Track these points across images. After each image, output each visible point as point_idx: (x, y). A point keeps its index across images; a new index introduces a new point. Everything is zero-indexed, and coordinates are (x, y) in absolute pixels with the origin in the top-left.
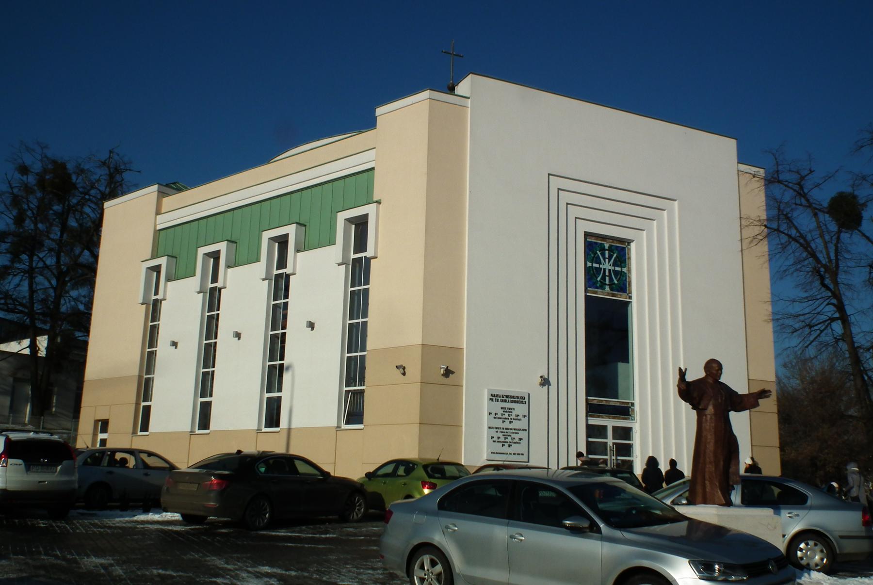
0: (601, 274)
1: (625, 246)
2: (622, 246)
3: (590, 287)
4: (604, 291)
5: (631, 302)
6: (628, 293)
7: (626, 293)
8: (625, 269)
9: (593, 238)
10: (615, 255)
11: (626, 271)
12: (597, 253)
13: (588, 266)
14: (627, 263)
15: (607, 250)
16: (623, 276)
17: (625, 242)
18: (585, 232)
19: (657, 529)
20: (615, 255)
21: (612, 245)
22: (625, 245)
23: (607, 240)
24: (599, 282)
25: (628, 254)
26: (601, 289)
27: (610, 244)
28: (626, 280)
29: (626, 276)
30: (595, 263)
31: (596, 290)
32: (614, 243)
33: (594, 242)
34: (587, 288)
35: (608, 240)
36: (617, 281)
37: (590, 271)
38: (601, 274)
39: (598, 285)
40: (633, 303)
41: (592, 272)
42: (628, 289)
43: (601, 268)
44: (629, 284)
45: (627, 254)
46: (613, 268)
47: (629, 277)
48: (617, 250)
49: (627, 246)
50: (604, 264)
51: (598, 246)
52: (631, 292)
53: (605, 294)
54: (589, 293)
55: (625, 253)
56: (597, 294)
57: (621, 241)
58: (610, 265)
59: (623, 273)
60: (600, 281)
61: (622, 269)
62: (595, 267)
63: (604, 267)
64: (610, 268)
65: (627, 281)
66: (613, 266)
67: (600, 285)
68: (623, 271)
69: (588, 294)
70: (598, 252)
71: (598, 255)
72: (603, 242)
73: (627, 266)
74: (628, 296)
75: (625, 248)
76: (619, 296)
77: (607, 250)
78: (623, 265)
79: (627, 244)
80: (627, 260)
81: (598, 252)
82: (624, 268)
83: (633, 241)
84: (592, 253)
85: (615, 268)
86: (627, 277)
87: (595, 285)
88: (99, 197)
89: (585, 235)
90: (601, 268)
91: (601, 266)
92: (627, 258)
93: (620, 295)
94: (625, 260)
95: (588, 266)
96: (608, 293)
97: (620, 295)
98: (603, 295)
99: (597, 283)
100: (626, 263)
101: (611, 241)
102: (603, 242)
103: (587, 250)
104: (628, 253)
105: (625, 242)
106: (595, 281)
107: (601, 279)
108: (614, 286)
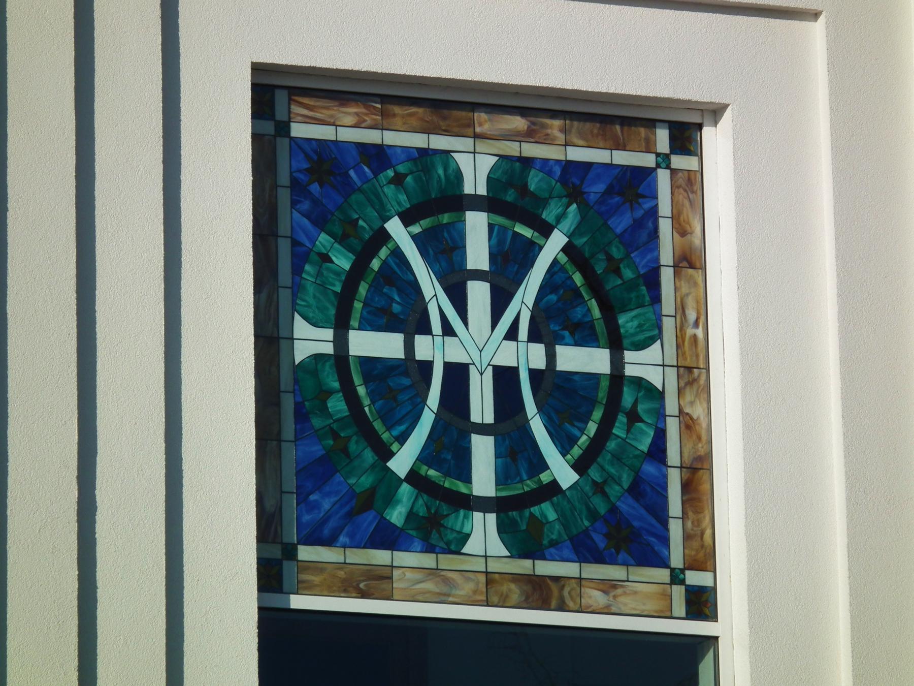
0: (427, 420)
1: (648, 160)
2: (622, 158)
3: (329, 542)
4: (447, 561)
5: (713, 640)
6: (677, 559)
7: (663, 563)
8: (653, 352)
9: (348, 114)
10: (556, 242)
11: (654, 377)
12: (384, 237)
13: (302, 352)
14: (668, 304)
15: (476, 203)
16: (633, 417)
17: (652, 124)
18: (257, 68)
19: (683, 318)
20: (556, 242)
21: (527, 162)
22: (649, 148)
23: (480, 116)
24: (405, 488)
25: (681, 229)
26: (429, 549)
27: (512, 149)
28: (658, 451)
29: (661, 415)
30: (593, 378)
31: (381, 557)
32: (547, 140)
33: (362, 147)
34: (290, 553)
35: (484, 122)
36: (579, 466)
37: (325, 394)
38: (427, 420)
39: (397, 516)
40: (723, 647)
41: (337, 405)
42: (675, 530)
43: (427, 367)
44: (687, 487)
45: (665, 227)
46: (536, 356)
47: (688, 425)
48: (575, 195)
49: (664, 161)
50: (448, 331)
51: (398, 180)
52: (711, 554)
53: (466, 588)
54: (303, 588)
55: (653, 213)
56: (389, 598)
57: (605, 120)
58: (512, 334)
59: (628, 399)
60: (413, 477)
61: (617, 363)
62: (367, 363)
63: (456, 355)
64: (507, 355)
65: (673, 455)
66: (534, 337)
67: (411, 515)
68: (629, 371)
69: (298, 602)
70: (394, 227)
71: (398, 254)
72: (439, 142)
73: (668, 325)
74: (678, 592)
75: (643, 175)
76: (596, 597)
77: (476, 203)
78: (626, 321)
79: (662, 138)
80: (667, 276)
81: (394, 227)
82: (640, 346)
83: (715, 112)
84: (342, 239)
85: (551, 357)
86: (673, 427)
87: (368, 520)
88: (306, 403)
89: (257, 88)
90: (427, 367)
91: (424, 347)
92: (666, 256)
93: (609, 586)
94: (652, 280)
95: (302, 352)
96: (490, 579)
97: (609, 586)
98: (441, 599)
99: (390, 500)
100: (656, 299)
101: (518, 123)
102: (439, 142)
103: (562, 343)
104: (676, 218)
105: (652, 124)
106: (365, 481)
107: (427, 456)
108: (547, 511)
